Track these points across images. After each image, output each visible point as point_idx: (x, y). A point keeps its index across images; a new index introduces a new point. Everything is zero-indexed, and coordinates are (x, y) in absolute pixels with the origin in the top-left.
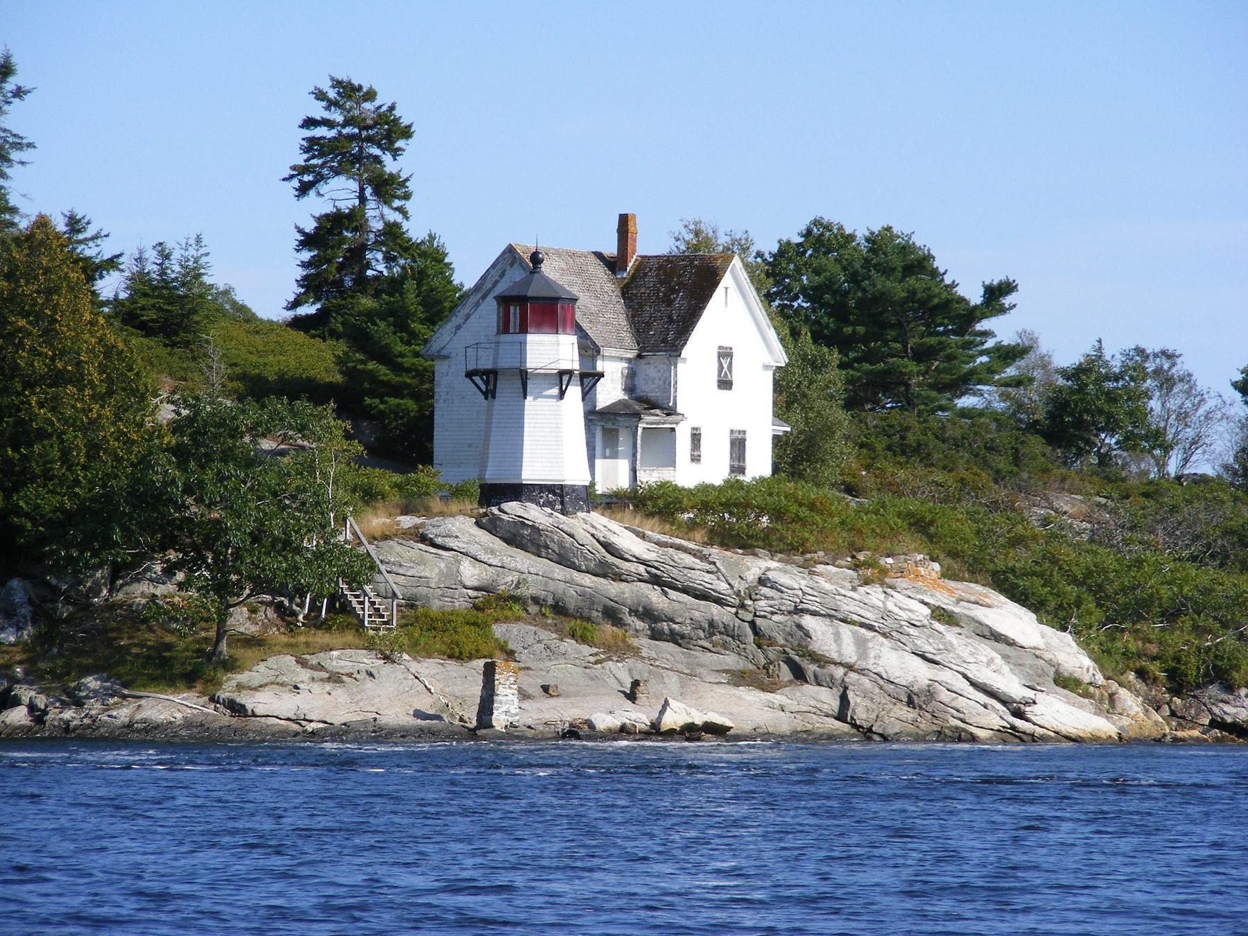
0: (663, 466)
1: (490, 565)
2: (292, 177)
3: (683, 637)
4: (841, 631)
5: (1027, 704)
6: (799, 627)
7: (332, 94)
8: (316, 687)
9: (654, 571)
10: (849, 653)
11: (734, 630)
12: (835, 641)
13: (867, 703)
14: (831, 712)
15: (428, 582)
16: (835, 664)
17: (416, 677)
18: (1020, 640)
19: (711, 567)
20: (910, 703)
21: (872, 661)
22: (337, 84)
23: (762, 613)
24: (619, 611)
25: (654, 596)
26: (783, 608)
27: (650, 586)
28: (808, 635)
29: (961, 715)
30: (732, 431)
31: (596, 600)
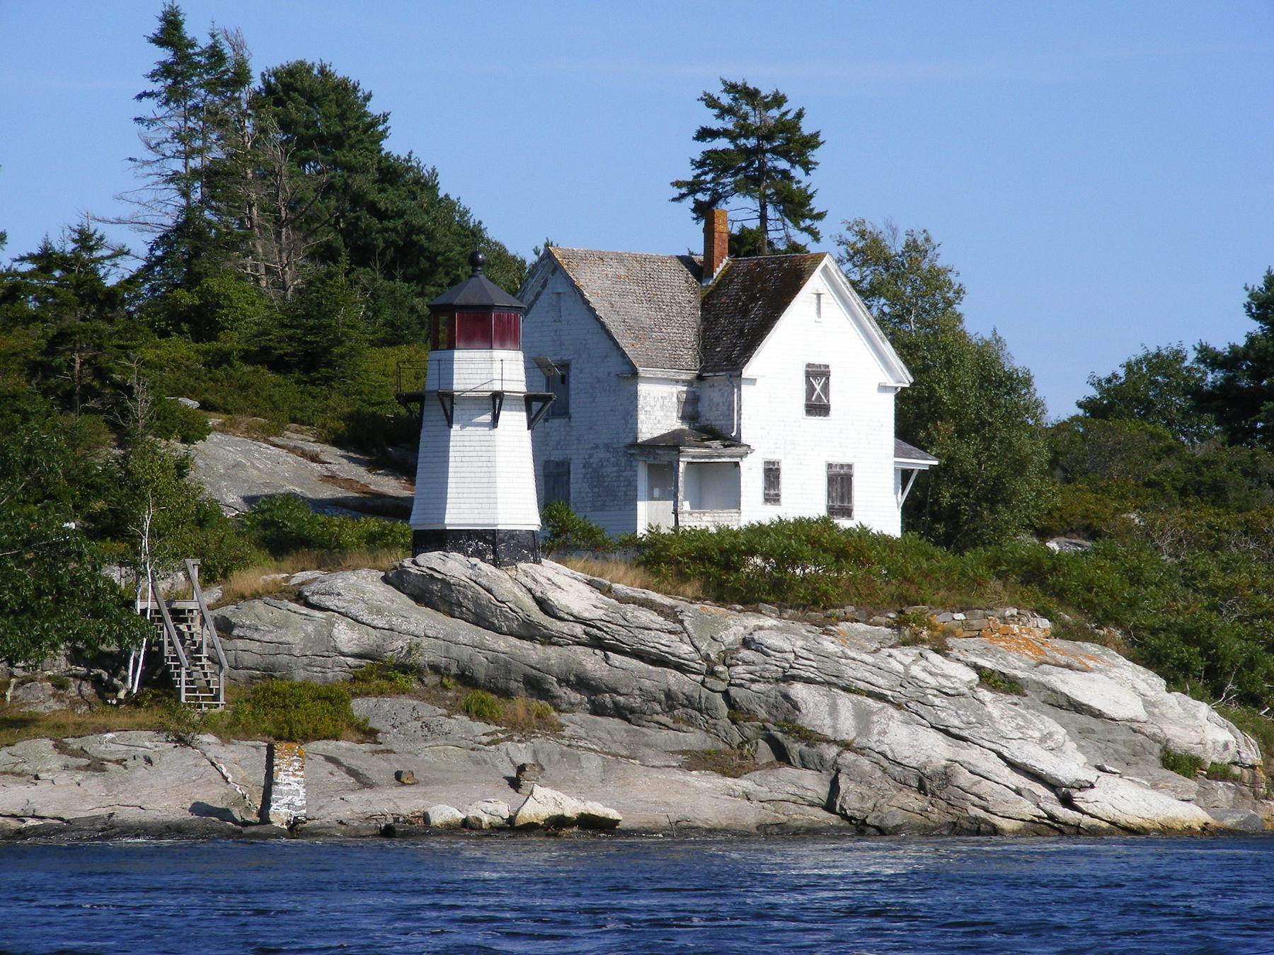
0: (723, 508)
1: (374, 628)
2: (683, 196)
3: (632, 711)
4: (839, 701)
5: (1081, 788)
6: (786, 697)
7: (726, 100)
8: (63, 778)
9: (595, 631)
10: (847, 727)
11: (700, 702)
12: (831, 714)
13: (864, 789)
14: (816, 801)
15: (290, 649)
16: (829, 741)
17: (213, 764)
18: (1109, 710)
19: (678, 627)
20: (921, 788)
21: (876, 738)
22: (731, 88)
23: (738, 681)
24: (545, 679)
25: (591, 663)
26: (767, 675)
27: (590, 650)
28: (796, 707)
29: (983, 803)
30: (830, 466)
31: (513, 668)
